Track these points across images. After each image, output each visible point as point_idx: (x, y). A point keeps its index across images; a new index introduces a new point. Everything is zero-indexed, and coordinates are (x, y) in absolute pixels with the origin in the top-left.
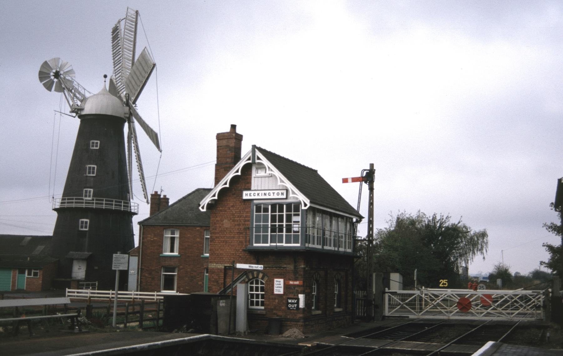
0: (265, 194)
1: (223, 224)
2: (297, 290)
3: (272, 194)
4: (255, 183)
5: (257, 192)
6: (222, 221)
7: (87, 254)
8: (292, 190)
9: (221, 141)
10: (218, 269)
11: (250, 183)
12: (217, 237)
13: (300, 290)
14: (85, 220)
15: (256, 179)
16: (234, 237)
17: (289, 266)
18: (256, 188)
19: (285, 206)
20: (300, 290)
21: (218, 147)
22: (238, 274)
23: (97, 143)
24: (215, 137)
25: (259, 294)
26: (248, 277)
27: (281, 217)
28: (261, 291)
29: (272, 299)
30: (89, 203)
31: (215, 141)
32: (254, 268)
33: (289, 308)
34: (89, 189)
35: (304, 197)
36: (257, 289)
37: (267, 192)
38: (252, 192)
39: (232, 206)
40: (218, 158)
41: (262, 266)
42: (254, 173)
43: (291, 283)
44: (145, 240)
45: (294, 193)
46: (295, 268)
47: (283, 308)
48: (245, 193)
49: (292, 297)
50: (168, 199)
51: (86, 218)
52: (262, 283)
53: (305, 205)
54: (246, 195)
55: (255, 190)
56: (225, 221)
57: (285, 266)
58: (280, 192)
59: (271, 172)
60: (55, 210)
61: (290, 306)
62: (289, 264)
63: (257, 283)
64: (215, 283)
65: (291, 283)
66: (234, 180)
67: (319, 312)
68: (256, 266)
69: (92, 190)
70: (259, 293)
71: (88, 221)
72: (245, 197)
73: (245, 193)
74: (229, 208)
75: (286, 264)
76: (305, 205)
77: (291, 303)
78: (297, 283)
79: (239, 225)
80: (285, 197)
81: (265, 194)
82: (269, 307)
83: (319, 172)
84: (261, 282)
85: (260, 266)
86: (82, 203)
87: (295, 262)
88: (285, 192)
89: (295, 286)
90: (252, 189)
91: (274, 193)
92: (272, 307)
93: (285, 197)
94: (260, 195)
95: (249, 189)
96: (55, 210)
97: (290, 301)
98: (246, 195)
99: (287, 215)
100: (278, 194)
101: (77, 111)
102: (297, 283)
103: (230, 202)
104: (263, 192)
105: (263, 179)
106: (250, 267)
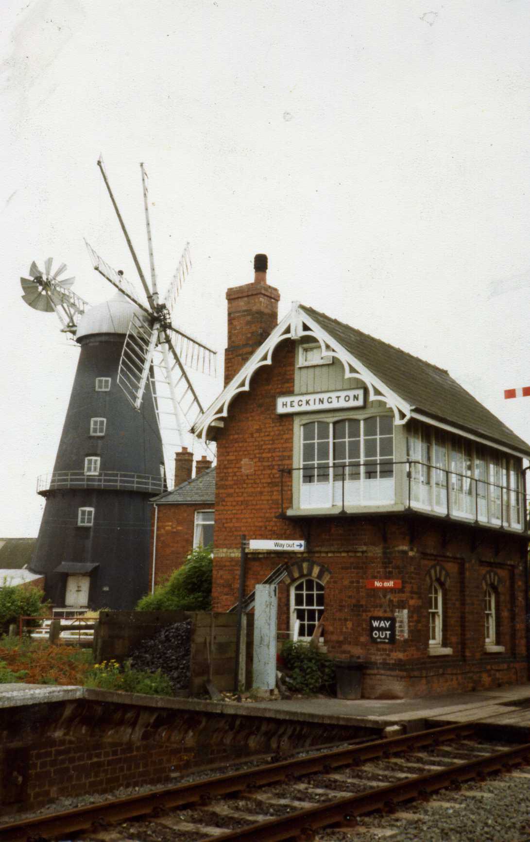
0: (321, 401)
1: (240, 468)
2: (391, 601)
3: (335, 400)
4: (300, 380)
5: (304, 398)
6: (238, 460)
7: (90, 566)
8: (350, 366)
9: (235, 303)
10: (232, 559)
11: (291, 380)
12: (229, 495)
13: (395, 600)
14: (87, 509)
15: (304, 371)
16: (261, 493)
17: (371, 548)
18: (304, 390)
19: (362, 423)
20: (395, 600)
21: (229, 314)
22: (271, 569)
23: (107, 382)
24: (225, 296)
25: (314, 611)
26: (290, 574)
27: (355, 447)
28: (317, 605)
29: (340, 620)
30: (93, 480)
31: (225, 303)
32: (286, 548)
33: (374, 641)
34: (94, 458)
35: (399, 399)
36: (310, 602)
37: (325, 396)
38: (296, 399)
39: (259, 431)
40: (230, 338)
41: (302, 542)
42: (302, 359)
43: (378, 584)
44: (163, 531)
45: (378, 392)
46: (384, 553)
47: (363, 639)
48: (280, 401)
49: (381, 614)
50: (191, 455)
51: (90, 506)
52: (320, 587)
53: (403, 416)
54: (284, 405)
55: (302, 394)
56: (245, 461)
57: (365, 548)
58: (351, 393)
59: (332, 354)
60: (42, 493)
61: (376, 634)
62: (374, 544)
63: (310, 587)
64: (226, 590)
65: (378, 584)
66: (260, 375)
67: (448, 651)
68: (290, 542)
69: (99, 459)
70: (315, 607)
71: (92, 509)
72: (281, 410)
73: (280, 401)
74: (252, 434)
75: (365, 544)
76: (403, 416)
77: (379, 629)
78: (390, 584)
79: (271, 467)
80: (360, 403)
81: (321, 401)
82: (334, 638)
83: (453, 375)
84: (318, 584)
85: (297, 542)
86: (83, 480)
87: (385, 539)
88: (360, 393)
89: (385, 590)
90: (296, 389)
91: (338, 397)
92: (341, 638)
93: (360, 403)
94: (311, 402)
95: (290, 392)
96: (42, 493)
97: (375, 624)
98: (284, 405)
99: (366, 441)
100: (347, 398)
101: (71, 328)
102: (390, 584)
103: (253, 423)
104: (318, 397)
105: (317, 370)
106: (276, 545)
